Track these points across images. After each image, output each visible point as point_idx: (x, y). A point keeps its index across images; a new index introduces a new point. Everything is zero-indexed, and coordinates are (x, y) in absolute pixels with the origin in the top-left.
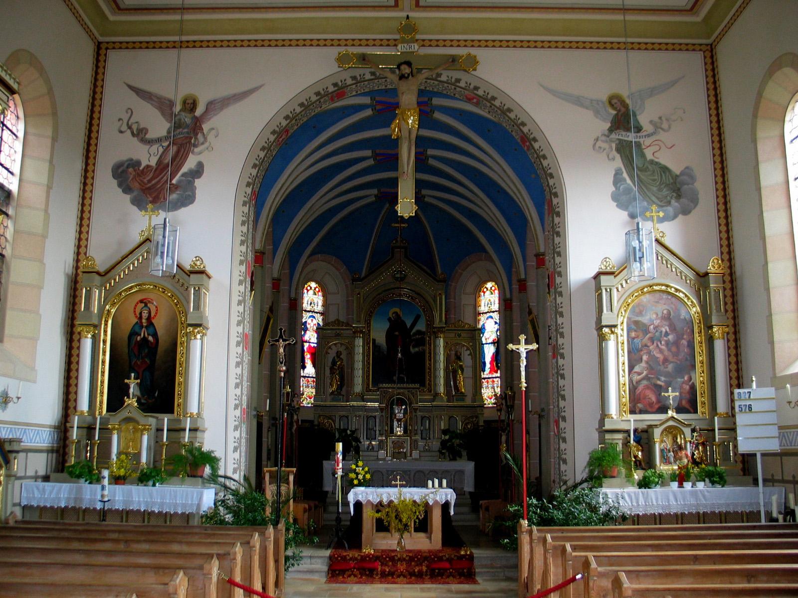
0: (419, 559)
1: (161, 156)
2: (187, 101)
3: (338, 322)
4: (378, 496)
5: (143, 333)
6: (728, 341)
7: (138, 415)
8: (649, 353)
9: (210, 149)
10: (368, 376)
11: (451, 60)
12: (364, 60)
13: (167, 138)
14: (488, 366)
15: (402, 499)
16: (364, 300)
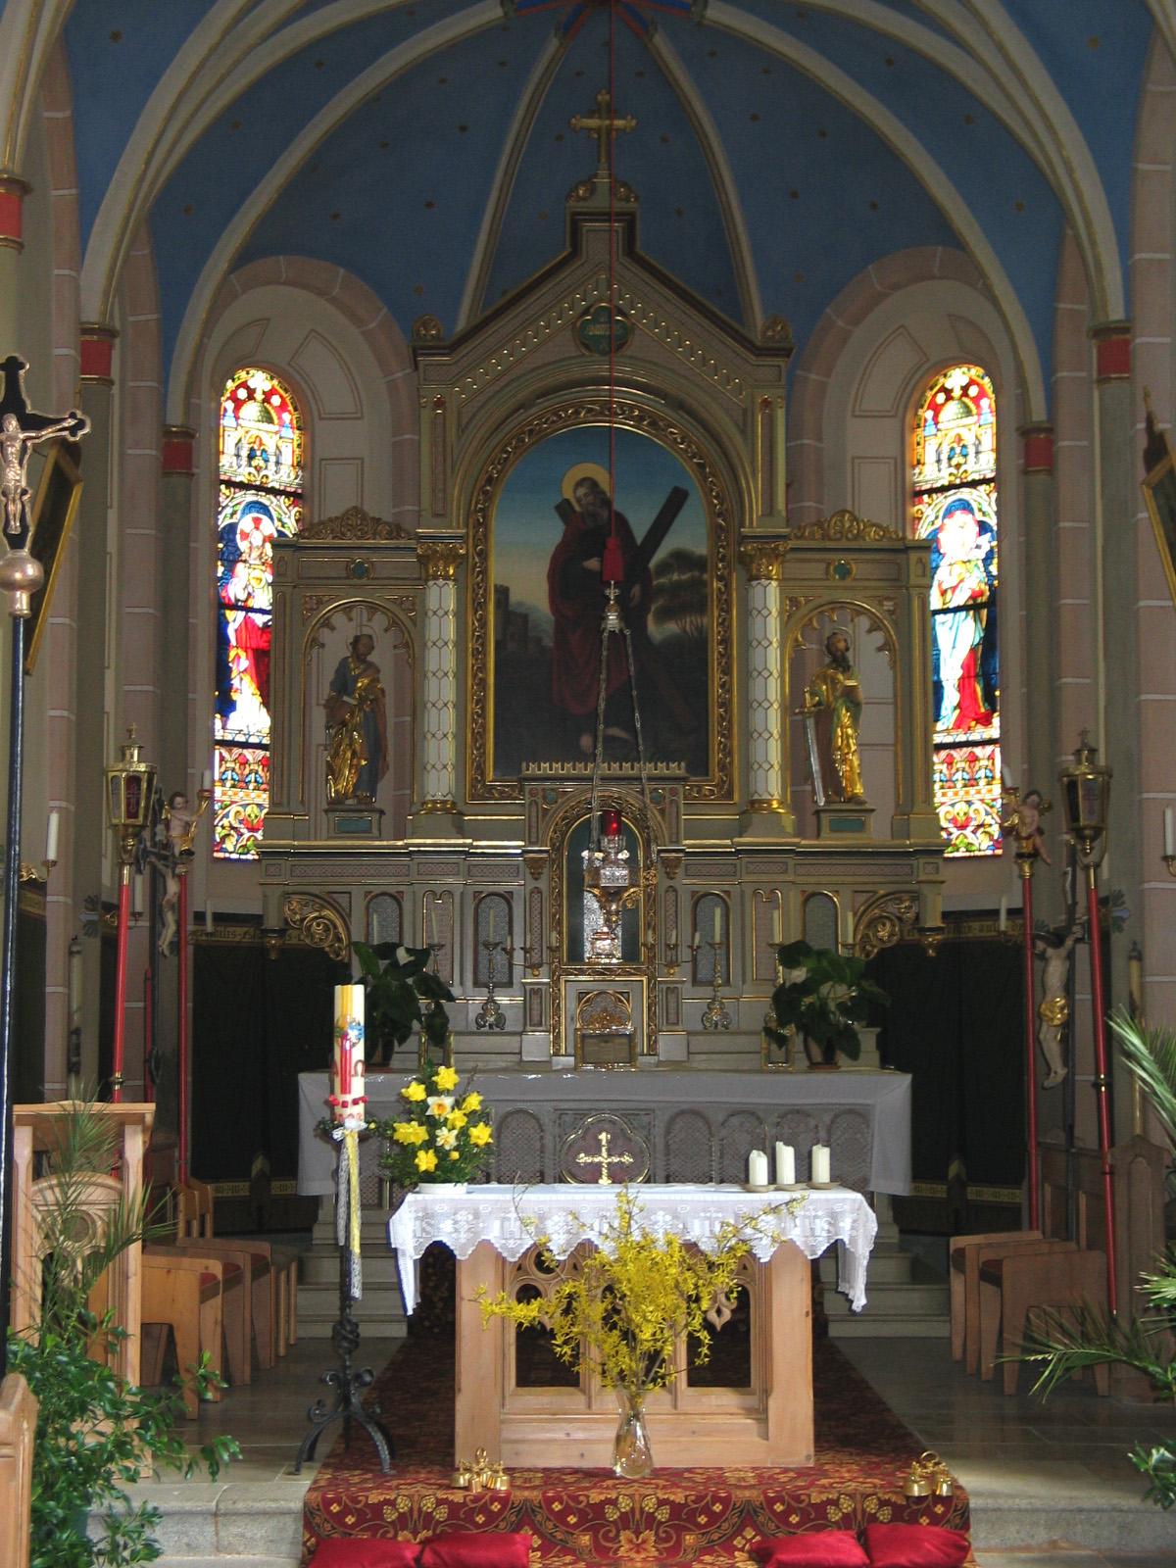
0: (714, 1518)
3: (356, 521)
4: (524, 1223)
10: (479, 736)
14: (951, 697)
15: (636, 1236)
16: (462, 430)
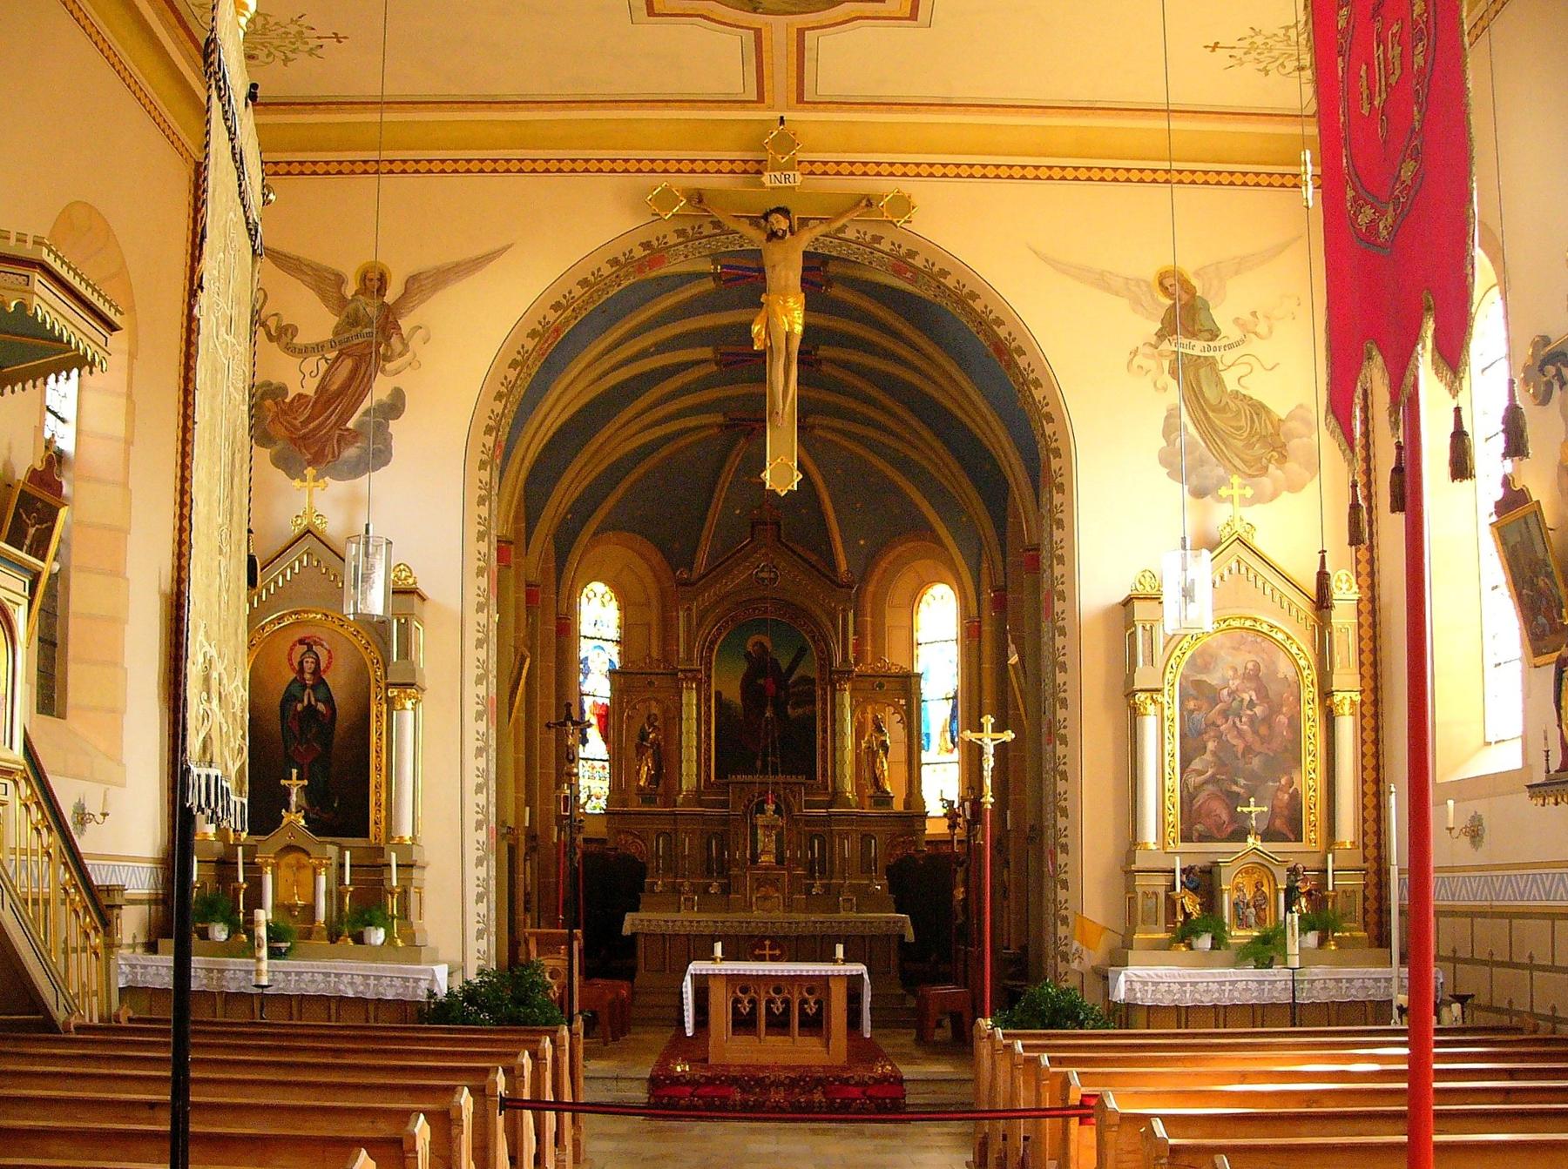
1: (323, 379)
2: (370, 275)
5: (308, 697)
6: (1363, 716)
7: (308, 840)
8: (1219, 737)
9: (415, 364)
11: (864, 203)
12: (700, 201)
13: (332, 344)
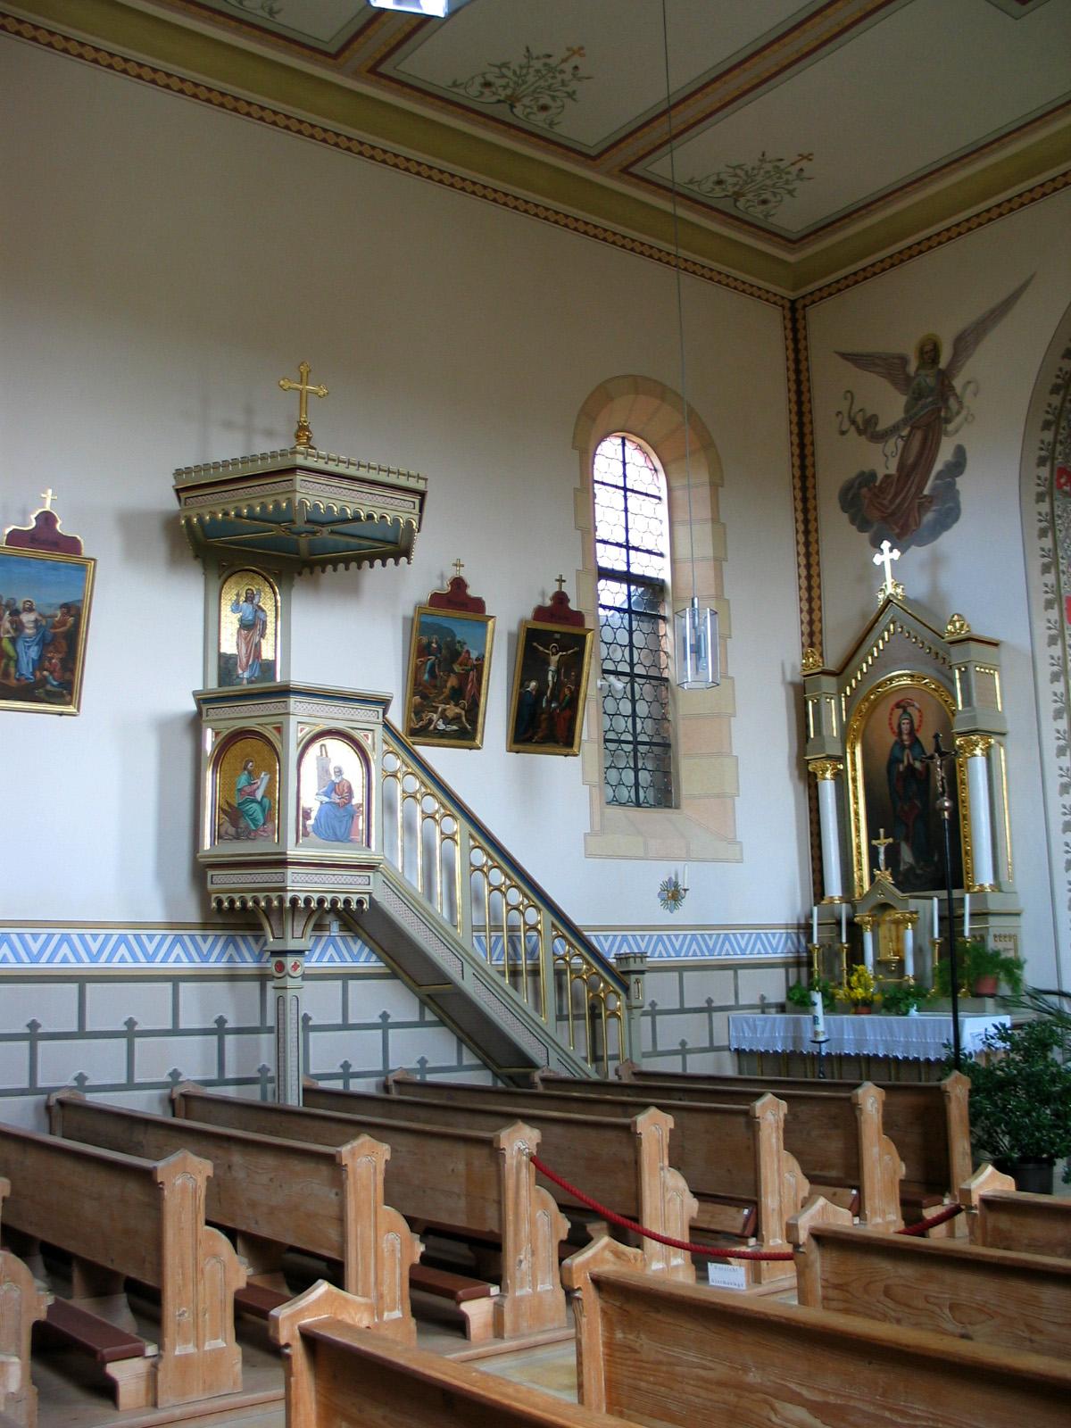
1: (902, 456)
9: (970, 418)
13: (905, 422)
